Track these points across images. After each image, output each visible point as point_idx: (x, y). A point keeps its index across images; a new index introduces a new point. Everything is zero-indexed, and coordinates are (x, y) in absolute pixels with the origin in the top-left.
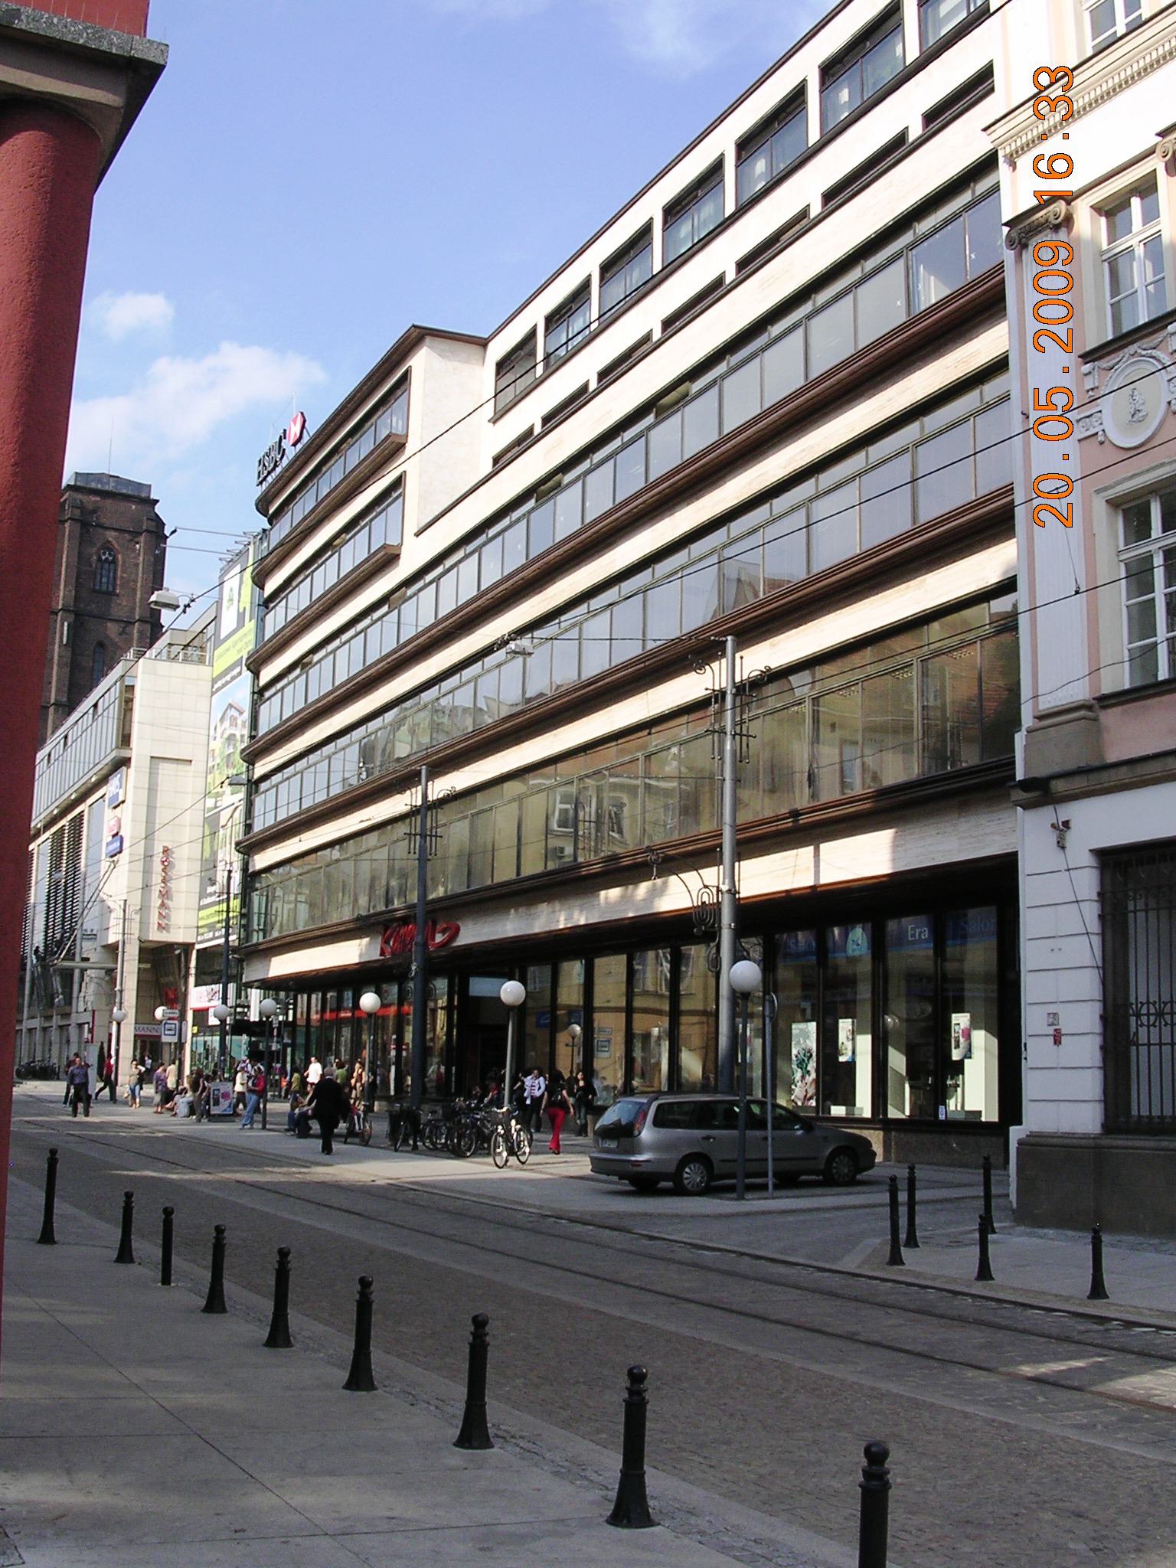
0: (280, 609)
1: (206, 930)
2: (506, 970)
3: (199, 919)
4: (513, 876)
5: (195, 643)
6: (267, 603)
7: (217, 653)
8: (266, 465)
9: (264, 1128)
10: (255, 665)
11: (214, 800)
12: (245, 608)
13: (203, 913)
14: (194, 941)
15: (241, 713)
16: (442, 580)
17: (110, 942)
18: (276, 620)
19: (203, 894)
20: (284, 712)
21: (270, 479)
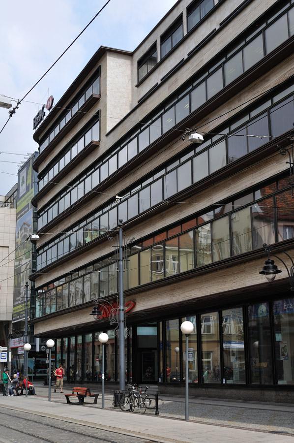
0: (46, 177)
1: (16, 315)
2: (155, 323)
3: (13, 311)
4: (137, 285)
5: (9, 201)
6: (41, 177)
7: (18, 203)
8: (36, 122)
9: (49, 400)
10: (35, 202)
11: (18, 262)
12: (29, 184)
13: (15, 308)
14: (11, 320)
15: (29, 226)
16: (119, 152)
17: (259, 190)
18: (44, 183)
19: (15, 301)
20: (60, 210)
21: (38, 126)
